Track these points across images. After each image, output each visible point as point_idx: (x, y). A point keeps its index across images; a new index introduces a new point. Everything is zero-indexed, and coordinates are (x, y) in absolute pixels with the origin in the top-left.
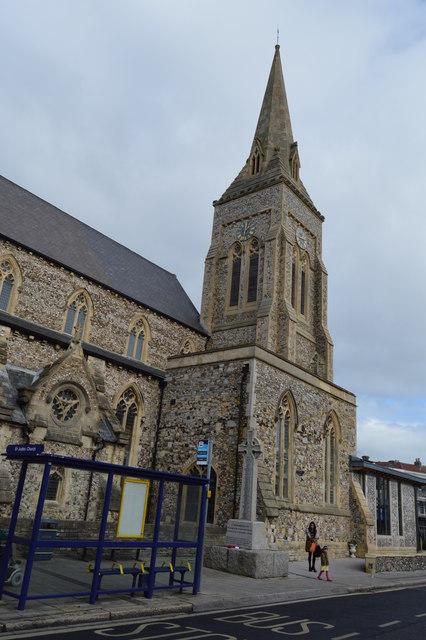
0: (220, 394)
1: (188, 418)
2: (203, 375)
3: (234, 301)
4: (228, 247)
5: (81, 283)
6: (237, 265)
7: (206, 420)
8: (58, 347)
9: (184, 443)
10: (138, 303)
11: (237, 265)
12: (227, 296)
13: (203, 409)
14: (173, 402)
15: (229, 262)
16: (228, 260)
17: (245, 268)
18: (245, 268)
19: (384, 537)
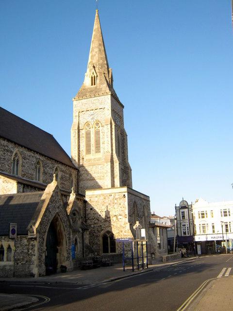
0: (113, 206)
2: (105, 198)
5: (38, 156)
10: (56, 161)
18: (93, 136)
19: (114, 254)
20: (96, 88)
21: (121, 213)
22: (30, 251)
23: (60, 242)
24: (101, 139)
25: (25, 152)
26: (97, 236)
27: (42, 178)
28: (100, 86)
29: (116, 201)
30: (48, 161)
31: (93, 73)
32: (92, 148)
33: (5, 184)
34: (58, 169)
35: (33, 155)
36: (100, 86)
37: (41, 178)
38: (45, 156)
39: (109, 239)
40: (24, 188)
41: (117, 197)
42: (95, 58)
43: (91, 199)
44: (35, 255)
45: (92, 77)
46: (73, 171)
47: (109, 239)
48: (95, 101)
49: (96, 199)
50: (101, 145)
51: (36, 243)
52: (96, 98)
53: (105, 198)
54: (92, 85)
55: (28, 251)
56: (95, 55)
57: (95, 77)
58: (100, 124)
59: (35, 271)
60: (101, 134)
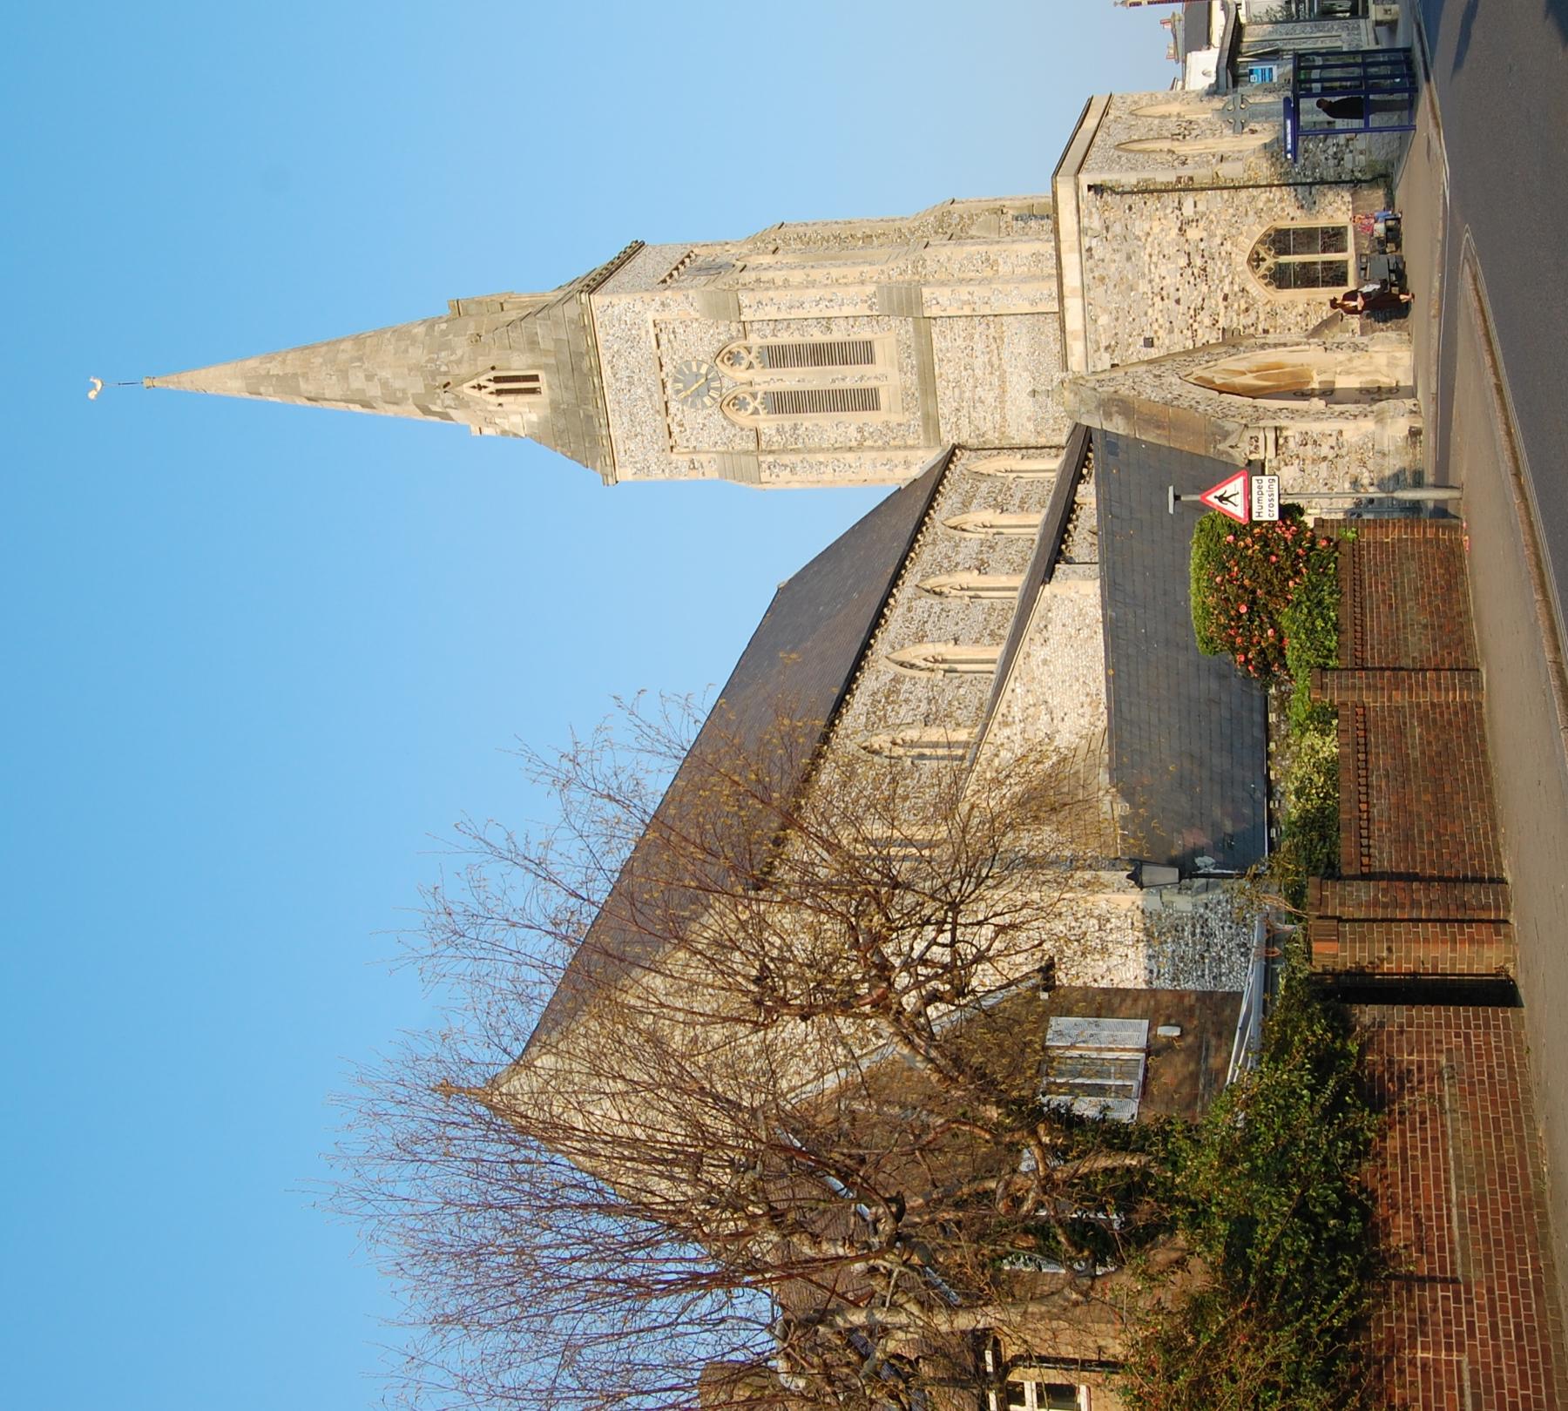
1: (1178, 301)
3: (867, 400)
4: (731, 431)
5: (903, 593)
6: (782, 403)
7: (1183, 262)
8: (1070, 527)
9: (1222, 304)
11: (782, 403)
12: (850, 423)
13: (1163, 271)
14: (1149, 343)
15: (768, 424)
16: (762, 426)
17: (792, 379)
18: (792, 379)
20: (556, 369)
21: (1058, 714)
22: (1325, 450)
23: (1292, 374)
24: (808, 340)
25: (892, 635)
26: (1273, 314)
27: (1004, 578)
28: (546, 353)
29: (1117, 228)
30: (926, 556)
31: (480, 387)
32: (848, 384)
33: (1055, 631)
34: (953, 521)
35: (899, 611)
36: (546, 353)
37: (1004, 581)
38: (902, 566)
39: (1284, 259)
40: (1069, 561)
41: (1096, 224)
42: (398, 384)
43: (1104, 344)
44: (1341, 432)
45: (499, 392)
46: (956, 469)
47: (1284, 259)
48: (623, 374)
49: (1104, 320)
50: (837, 336)
51: (1293, 430)
52: (607, 372)
53: (1102, 279)
54: (533, 391)
55: (1325, 458)
56: (385, 384)
57: (497, 380)
58: (733, 347)
59: (1399, 428)
60: (785, 338)
